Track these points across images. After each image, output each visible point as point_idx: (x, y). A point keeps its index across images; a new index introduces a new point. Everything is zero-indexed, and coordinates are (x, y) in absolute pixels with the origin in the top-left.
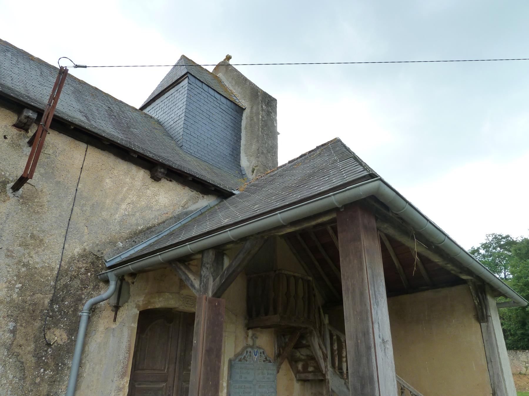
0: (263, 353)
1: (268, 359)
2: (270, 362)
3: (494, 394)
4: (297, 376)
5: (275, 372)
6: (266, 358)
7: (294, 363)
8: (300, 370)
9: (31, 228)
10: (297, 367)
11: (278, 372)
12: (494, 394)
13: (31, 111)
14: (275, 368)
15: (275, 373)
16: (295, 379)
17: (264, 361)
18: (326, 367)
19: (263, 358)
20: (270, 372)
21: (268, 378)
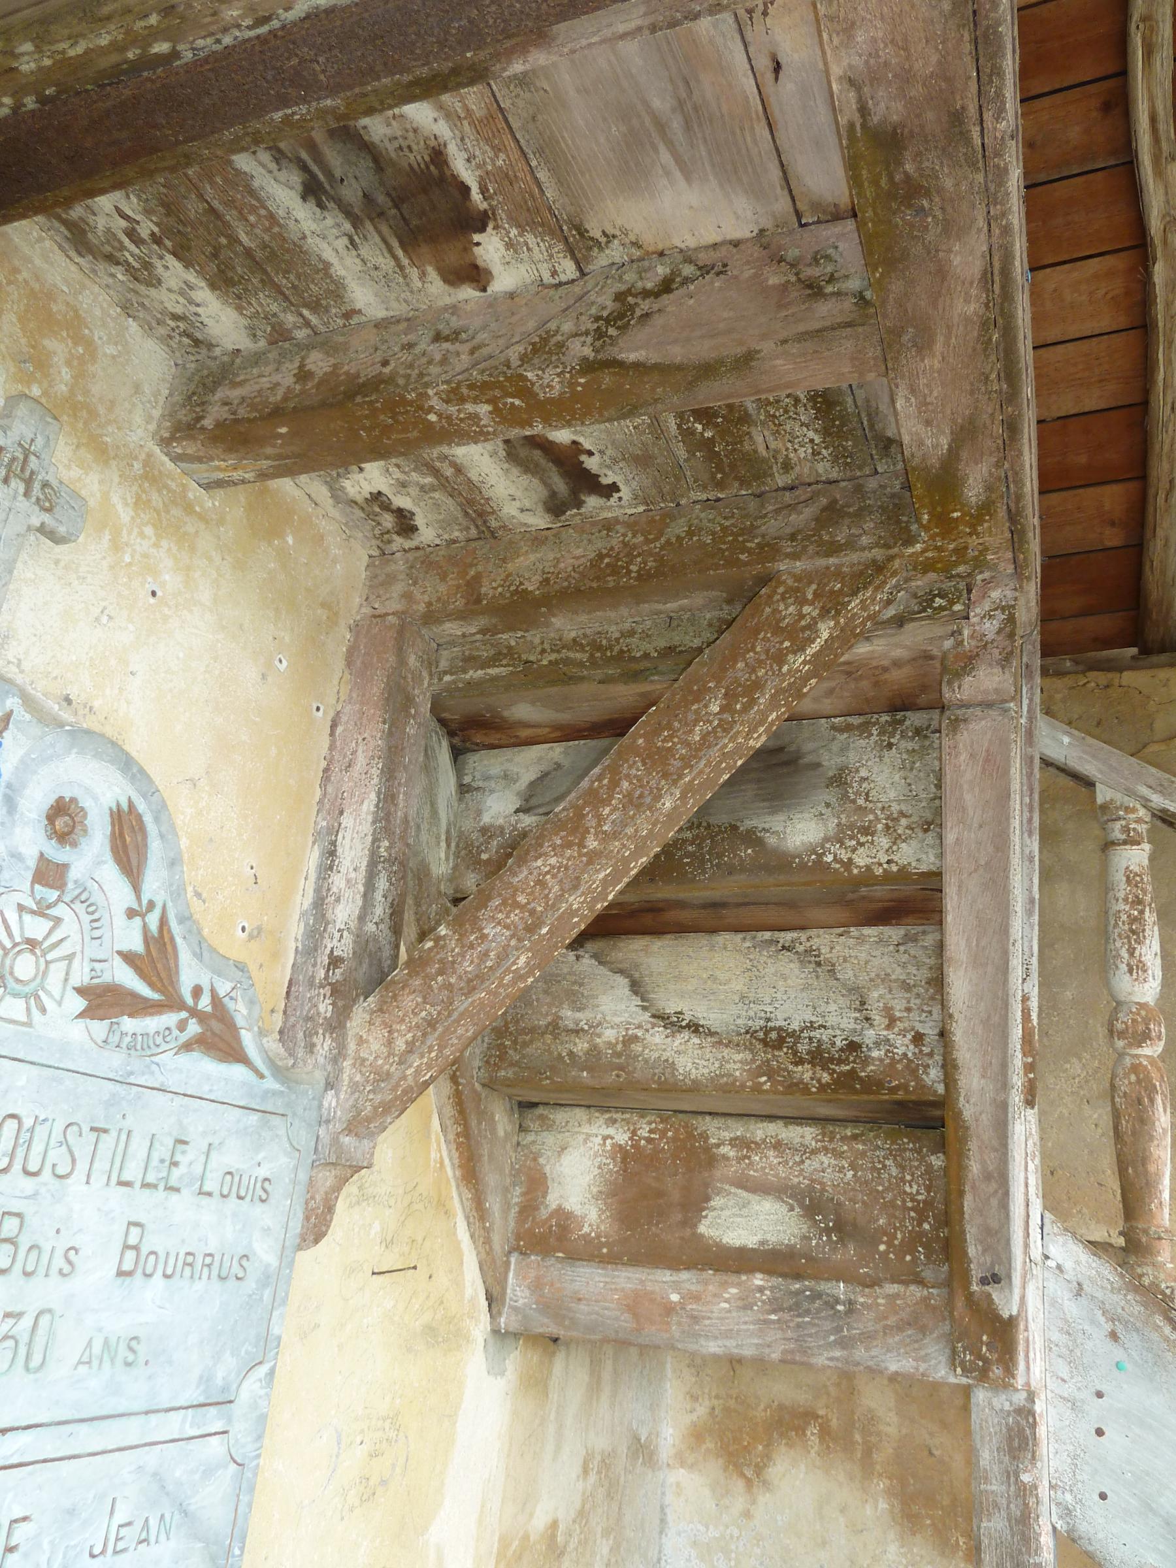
0: (128, 842)
1: (190, 974)
2: (219, 1039)
3: (4, 1431)
4: (517, 1291)
5: (264, 1231)
6: (154, 961)
7: (502, 1120)
8: (564, 1220)
9: (127, 559)
10: (536, 1184)
11: (316, 1226)
12: (4, 1431)
13: (759, 1276)
14: (278, 1161)
15: (266, 1253)
16: (480, 1327)
17: (103, 1001)
18: (219, 469)
19: (102, 931)
20: (189, 1222)
21: (130, 1352)
